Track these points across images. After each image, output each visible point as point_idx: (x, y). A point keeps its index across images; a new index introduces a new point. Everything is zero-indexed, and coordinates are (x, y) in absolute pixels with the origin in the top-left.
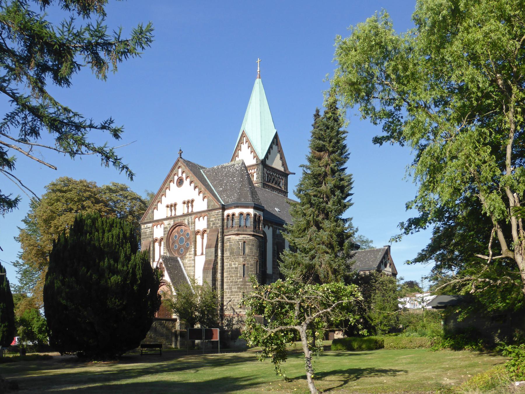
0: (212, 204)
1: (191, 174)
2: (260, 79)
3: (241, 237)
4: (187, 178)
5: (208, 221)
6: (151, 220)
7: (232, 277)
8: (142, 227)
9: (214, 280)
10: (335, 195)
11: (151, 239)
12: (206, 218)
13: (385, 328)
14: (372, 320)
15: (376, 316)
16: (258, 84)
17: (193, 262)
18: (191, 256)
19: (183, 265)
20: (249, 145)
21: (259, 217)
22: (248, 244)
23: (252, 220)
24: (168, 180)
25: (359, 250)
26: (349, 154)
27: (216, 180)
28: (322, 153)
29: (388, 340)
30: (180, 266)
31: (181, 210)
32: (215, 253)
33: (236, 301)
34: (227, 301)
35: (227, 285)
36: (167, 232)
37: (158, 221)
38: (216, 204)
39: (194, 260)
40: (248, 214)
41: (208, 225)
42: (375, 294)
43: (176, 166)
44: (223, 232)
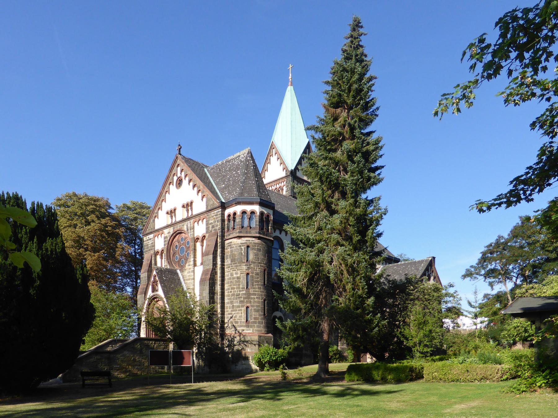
0: (211, 203)
1: (189, 172)
2: (292, 87)
3: (244, 240)
4: (186, 176)
5: (207, 224)
6: (152, 230)
7: (234, 289)
8: (145, 239)
9: (212, 293)
10: (354, 162)
11: (152, 252)
12: (205, 220)
13: (425, 350)
14: (407, 339)
15: (413, 333)
16: (290, 92)
17: (192, 274)
18: (190, 267)
19: (183, 278)
20: (279, 157)
21: (268, 216)
22: (253, 249)
23: (258, 219)
24: (167, 182)
25: (399, 263)
26: (378, 109)
27: (219, 177)
28: (339, 110)
29: (430, 367)
30: (179, 280)
31: (181, 214)
32: (213, 261)
33: (238, 317)
34: (228, 318)
35: (228, 299)
36: (167, 242)
37: (158, 230)
38: (215, 202)
39: (194, 271)
40: (253, 213)
41: (207, 228)
42: (414, 305)
43: (175, 164)
44: (223, 236)
